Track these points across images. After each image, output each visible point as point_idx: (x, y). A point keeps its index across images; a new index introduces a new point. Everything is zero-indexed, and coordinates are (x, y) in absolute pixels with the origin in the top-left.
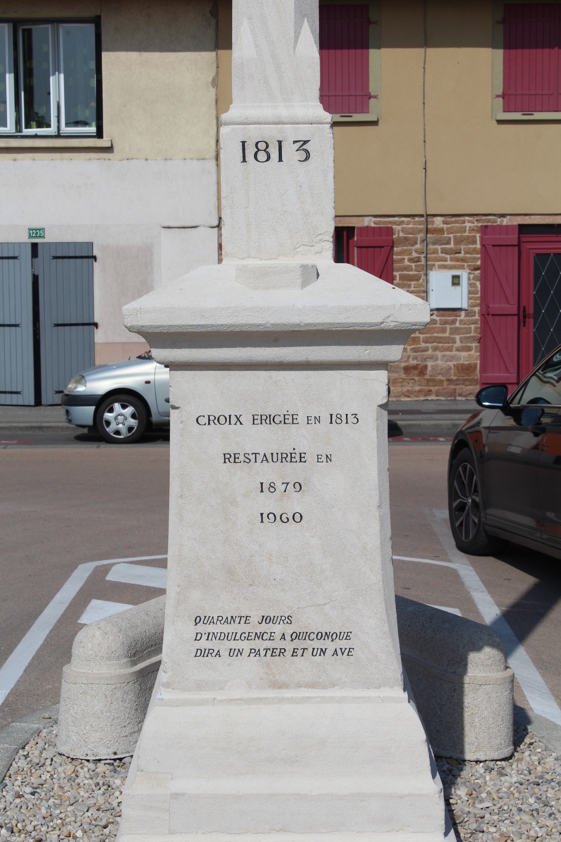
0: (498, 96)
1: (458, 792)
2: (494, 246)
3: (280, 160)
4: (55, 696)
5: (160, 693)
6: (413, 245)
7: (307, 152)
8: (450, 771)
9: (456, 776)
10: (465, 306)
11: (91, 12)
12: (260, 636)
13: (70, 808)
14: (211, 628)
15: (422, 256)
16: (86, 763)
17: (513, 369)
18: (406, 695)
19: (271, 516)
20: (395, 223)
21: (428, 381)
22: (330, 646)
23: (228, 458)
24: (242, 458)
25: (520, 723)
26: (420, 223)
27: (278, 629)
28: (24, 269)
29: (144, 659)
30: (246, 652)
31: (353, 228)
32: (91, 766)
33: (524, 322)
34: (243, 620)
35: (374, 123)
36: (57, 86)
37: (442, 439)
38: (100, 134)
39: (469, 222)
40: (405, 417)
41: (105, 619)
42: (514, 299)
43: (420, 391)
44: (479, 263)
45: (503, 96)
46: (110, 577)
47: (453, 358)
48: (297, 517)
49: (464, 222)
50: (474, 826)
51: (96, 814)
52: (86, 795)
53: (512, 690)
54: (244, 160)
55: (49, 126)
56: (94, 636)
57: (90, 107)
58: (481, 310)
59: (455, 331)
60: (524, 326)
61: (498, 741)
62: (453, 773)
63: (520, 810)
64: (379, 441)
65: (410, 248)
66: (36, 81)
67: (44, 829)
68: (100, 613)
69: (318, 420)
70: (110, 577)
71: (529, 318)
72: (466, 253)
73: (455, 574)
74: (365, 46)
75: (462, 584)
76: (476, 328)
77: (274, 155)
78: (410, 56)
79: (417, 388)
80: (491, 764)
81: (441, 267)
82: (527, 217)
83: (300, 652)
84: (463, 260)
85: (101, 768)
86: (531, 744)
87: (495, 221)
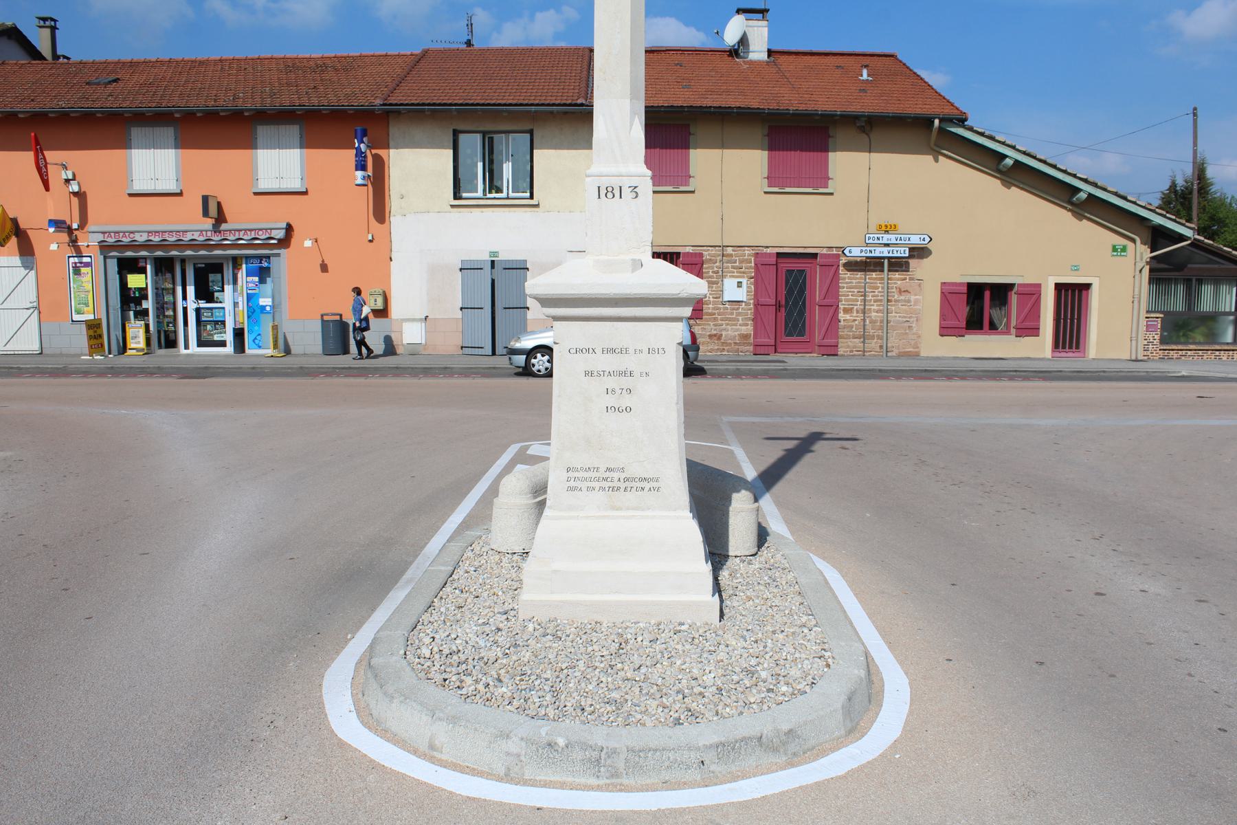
4: (489, 518)
11: (528, 127)
12: (605, 479)
14: (576, 474)
22: (647, 485)
23: (586, 373)
25: (762, 535)
27: (616, 475)
28: (487, 274)
35: (693, 192)
36: (507, 170)
38: (532, 197)
57: (528, 181)
59: (739, 314)
66: (495, 167)
69: (641, 351)
73: (732, 452)
74: (686, 146)
77: (617, 195)
78: (714, 154)
85: (515, 557)
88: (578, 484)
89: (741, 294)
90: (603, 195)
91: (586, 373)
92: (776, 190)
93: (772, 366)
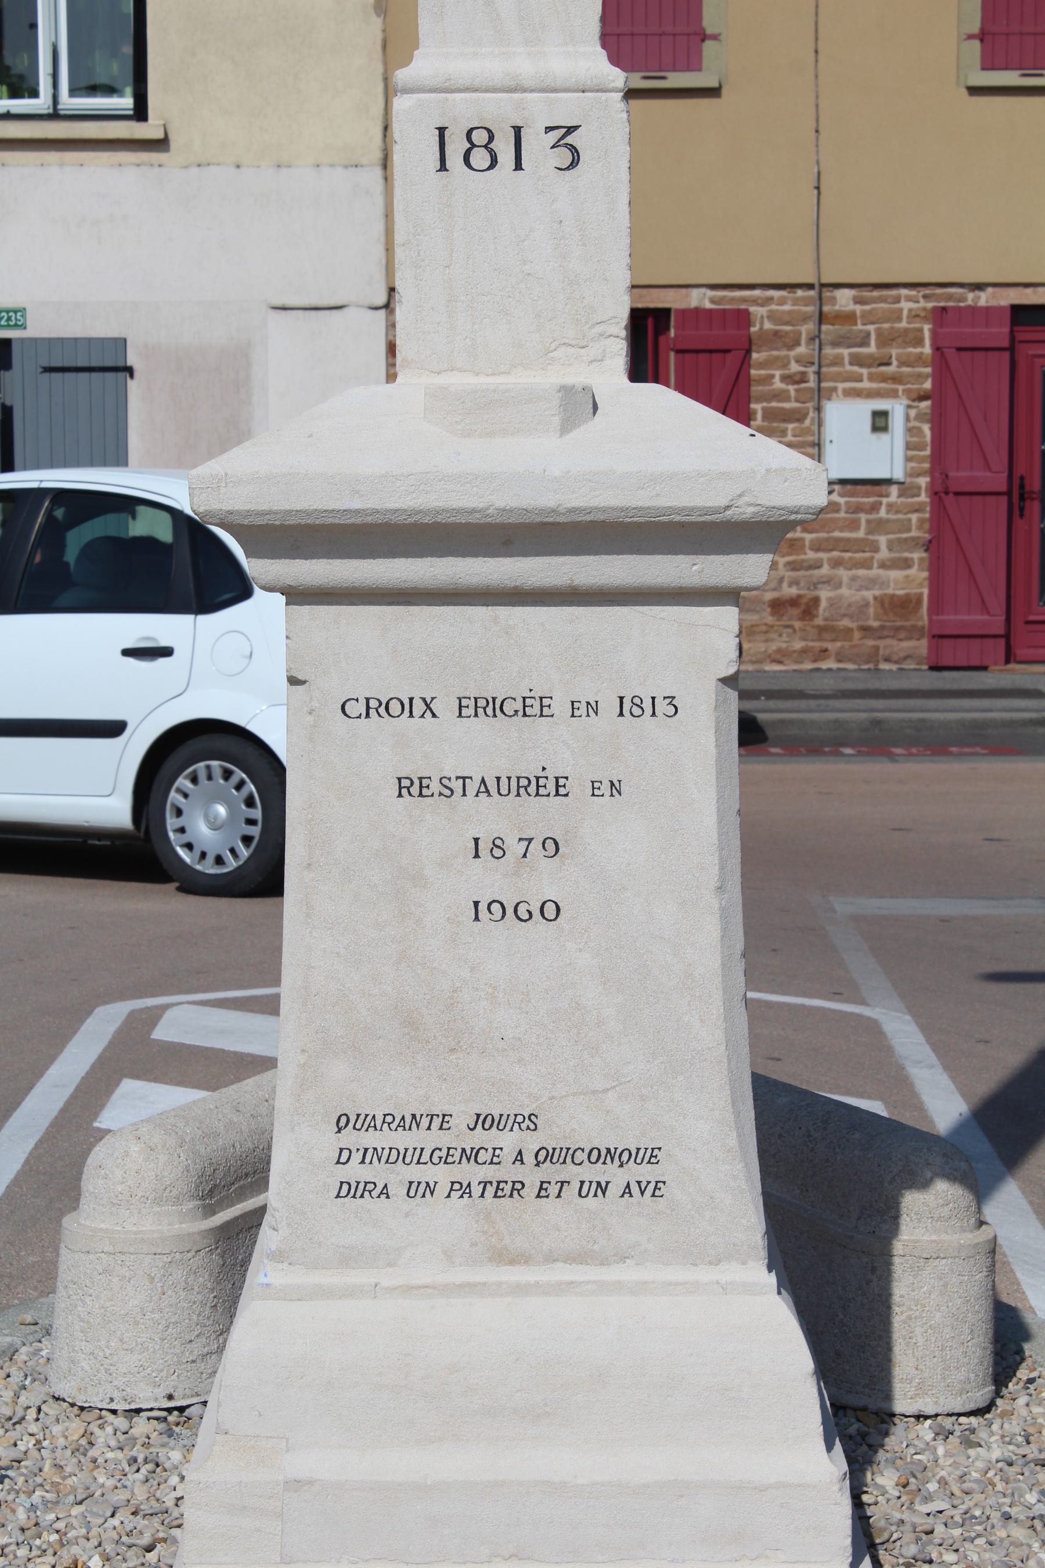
0: (970, 37)
1: (879, 1480)
2: (959, 349)
3: (518, 166)
5: (264, 1273)
6: (791, 348)
7: (574, 150)
8: (864, 1436)
9: (875, 1448)
10: (898, 474)
12: (471, 1156)
13: (76, 1511)
14: (371, 1139)
15: (811, 370)
16: (110, 1417)
17: (997, 604)
18: (772, 1279)
19: (496, 907)
20: (755, 302)
21: (821, 629)
22: (617, 1176)
23: (404, 786)
24: (435, 787)
26: (807, 302)
27: (508, 1141)
29: (231, 1198)
30: (442, 1189)
31: (667, 312)
32: (121, 1422)
33: (1022, 509)
34: (437, 1122)
35: (713, 92)
37: (848, 751)
38: (140, 113)
39: (909, 299)
40: (772, 704)
41: (149, 1120)
42: (999, 460)
43: (804, 651)
44: (928, 385)
45: (982, 36)
46: (160, 1033)
47: (873, 582)
48: (550, 911)
49: (897, 300)
50: (912, 1550)
51: (130, 1522)
52: (110, 1483)
53: (992, 1269)
54: (443, 167)
55: (34, 94)
56: (127, 1154)
58: (932, 484)
60: (1022, 516)
61: (962, 1375)
62: (871, 1440)
63: (1007, 1517)
64: (719, 754)
65: (784, 353)
67: (22, 1552)
68: (139, 1105)
69: (593, 708)
70: (160, 1033)
71: (1032, 499)
72: (902, 364)
73: (873, 1028)
75: (889, 1050)
76: (921, 521)
77: (506, 157)
79: (798, 645)
80: (947, 1423)
81: (850, 393)
82: (1029, 291)
83: (554, 1190)
84: (896, 379)
85: (141, 1426)
86: (1031, 1381)
87: (963, 299)
88: (375, 1173)
89: (886, 457)
90: (454, 159)
91: (404, 786)
92: (1010, 78)
93: (999, 710)
